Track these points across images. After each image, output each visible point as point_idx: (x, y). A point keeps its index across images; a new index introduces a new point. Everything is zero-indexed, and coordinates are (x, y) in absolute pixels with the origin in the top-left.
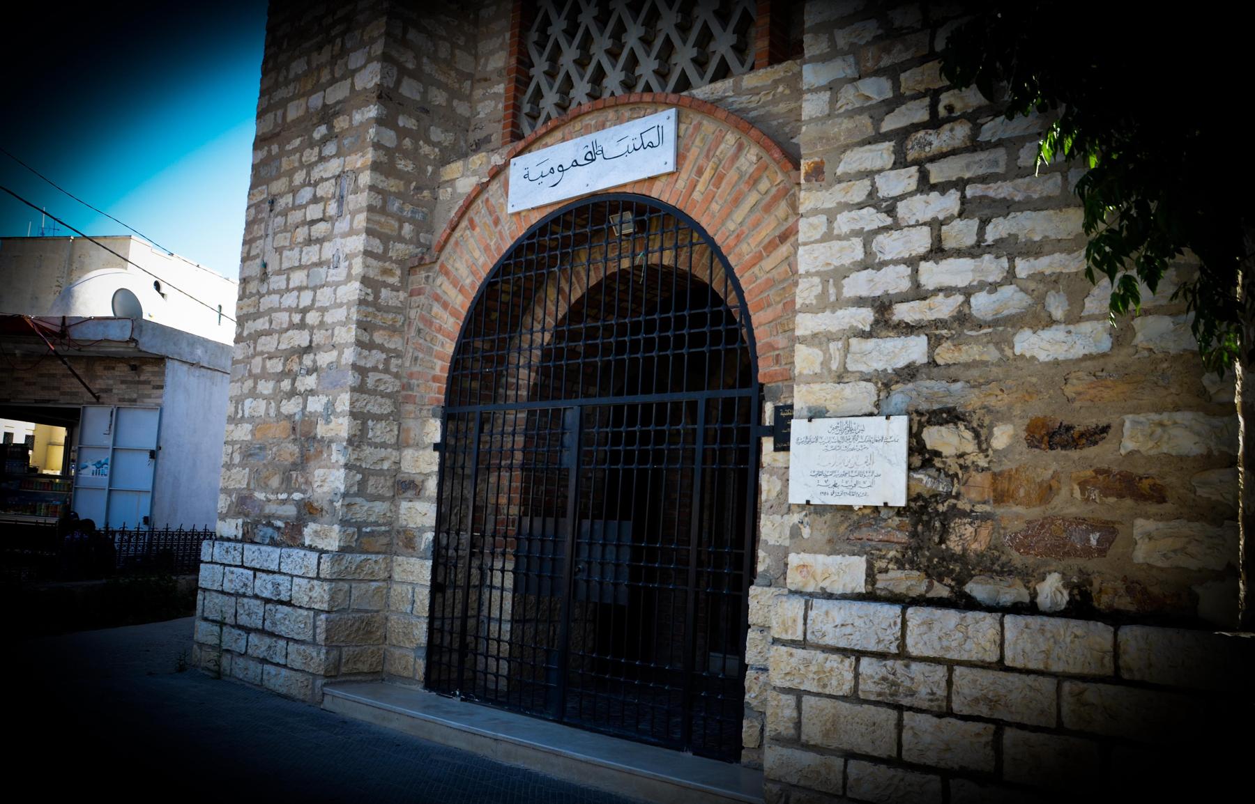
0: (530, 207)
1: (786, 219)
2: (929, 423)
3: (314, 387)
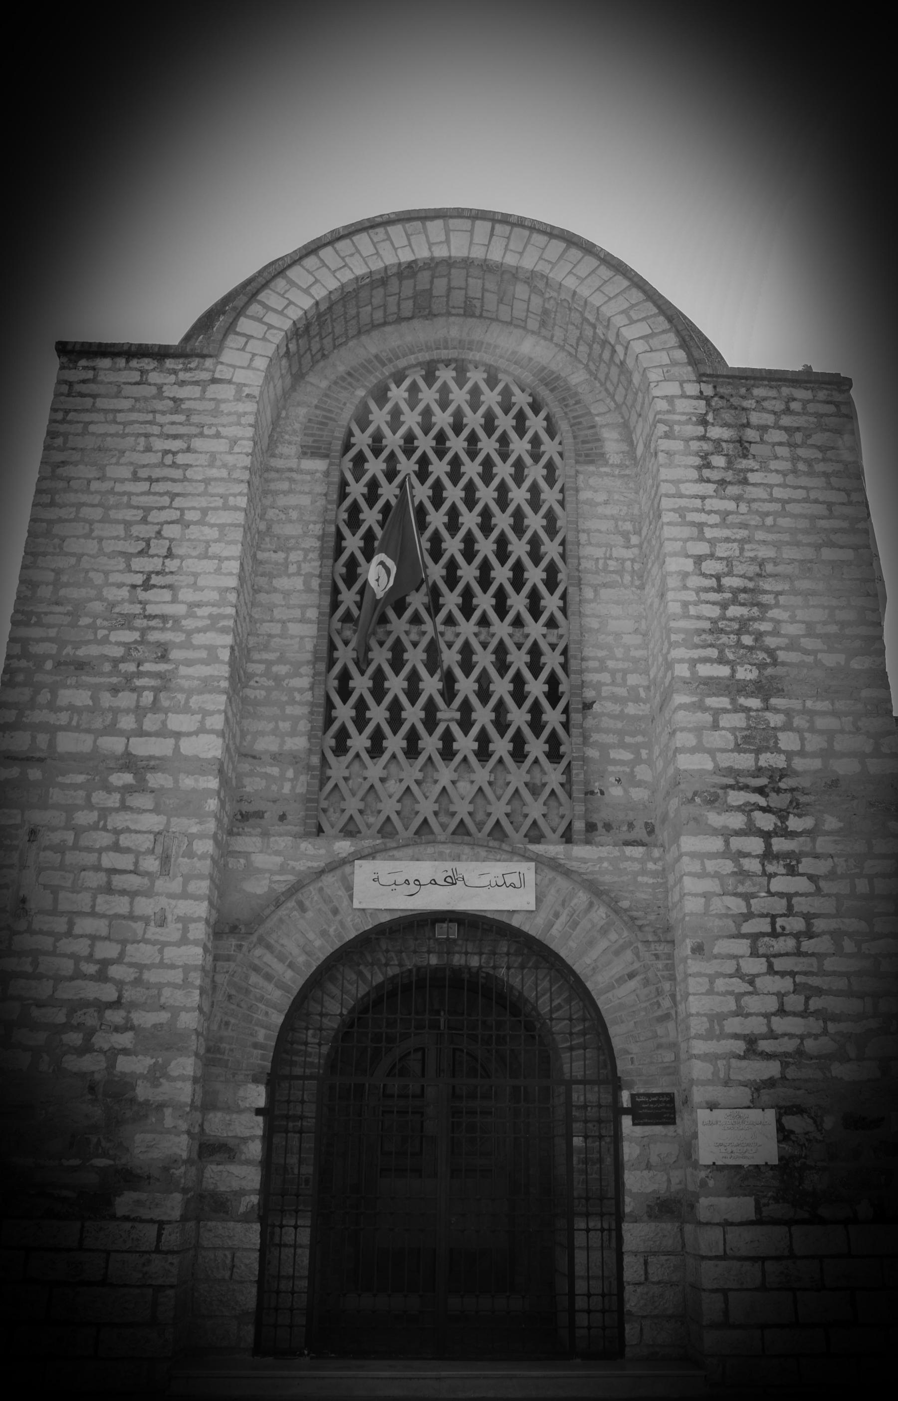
2: (786, 1113)
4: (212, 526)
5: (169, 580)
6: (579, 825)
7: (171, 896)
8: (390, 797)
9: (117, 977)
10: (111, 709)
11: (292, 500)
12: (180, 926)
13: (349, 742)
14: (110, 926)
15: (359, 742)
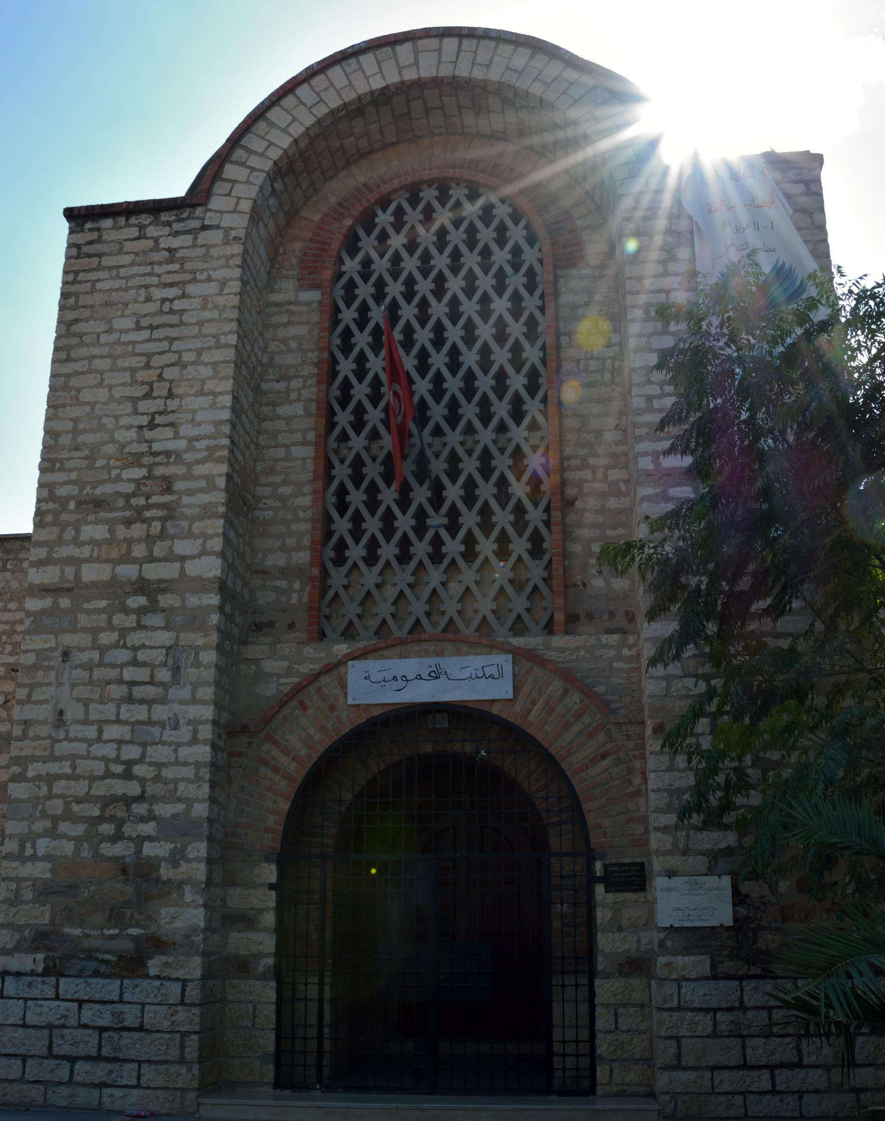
0: (373, 702)
1: (605, 744)
3: (153, 833)
4: (206, 364)
5: (170, 418)
6: (559, 617)
7: (182, 702)
8: (385, 601)
9: (140, 775)
10: (125, 539)
11: (291, 331)
12: (191, 728)
13: (347, 553)
14: (132, 732)
15: (356, 552)
